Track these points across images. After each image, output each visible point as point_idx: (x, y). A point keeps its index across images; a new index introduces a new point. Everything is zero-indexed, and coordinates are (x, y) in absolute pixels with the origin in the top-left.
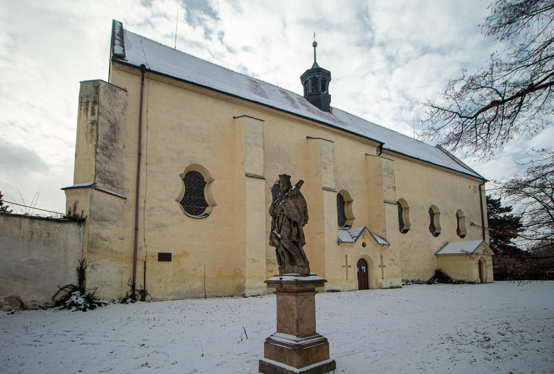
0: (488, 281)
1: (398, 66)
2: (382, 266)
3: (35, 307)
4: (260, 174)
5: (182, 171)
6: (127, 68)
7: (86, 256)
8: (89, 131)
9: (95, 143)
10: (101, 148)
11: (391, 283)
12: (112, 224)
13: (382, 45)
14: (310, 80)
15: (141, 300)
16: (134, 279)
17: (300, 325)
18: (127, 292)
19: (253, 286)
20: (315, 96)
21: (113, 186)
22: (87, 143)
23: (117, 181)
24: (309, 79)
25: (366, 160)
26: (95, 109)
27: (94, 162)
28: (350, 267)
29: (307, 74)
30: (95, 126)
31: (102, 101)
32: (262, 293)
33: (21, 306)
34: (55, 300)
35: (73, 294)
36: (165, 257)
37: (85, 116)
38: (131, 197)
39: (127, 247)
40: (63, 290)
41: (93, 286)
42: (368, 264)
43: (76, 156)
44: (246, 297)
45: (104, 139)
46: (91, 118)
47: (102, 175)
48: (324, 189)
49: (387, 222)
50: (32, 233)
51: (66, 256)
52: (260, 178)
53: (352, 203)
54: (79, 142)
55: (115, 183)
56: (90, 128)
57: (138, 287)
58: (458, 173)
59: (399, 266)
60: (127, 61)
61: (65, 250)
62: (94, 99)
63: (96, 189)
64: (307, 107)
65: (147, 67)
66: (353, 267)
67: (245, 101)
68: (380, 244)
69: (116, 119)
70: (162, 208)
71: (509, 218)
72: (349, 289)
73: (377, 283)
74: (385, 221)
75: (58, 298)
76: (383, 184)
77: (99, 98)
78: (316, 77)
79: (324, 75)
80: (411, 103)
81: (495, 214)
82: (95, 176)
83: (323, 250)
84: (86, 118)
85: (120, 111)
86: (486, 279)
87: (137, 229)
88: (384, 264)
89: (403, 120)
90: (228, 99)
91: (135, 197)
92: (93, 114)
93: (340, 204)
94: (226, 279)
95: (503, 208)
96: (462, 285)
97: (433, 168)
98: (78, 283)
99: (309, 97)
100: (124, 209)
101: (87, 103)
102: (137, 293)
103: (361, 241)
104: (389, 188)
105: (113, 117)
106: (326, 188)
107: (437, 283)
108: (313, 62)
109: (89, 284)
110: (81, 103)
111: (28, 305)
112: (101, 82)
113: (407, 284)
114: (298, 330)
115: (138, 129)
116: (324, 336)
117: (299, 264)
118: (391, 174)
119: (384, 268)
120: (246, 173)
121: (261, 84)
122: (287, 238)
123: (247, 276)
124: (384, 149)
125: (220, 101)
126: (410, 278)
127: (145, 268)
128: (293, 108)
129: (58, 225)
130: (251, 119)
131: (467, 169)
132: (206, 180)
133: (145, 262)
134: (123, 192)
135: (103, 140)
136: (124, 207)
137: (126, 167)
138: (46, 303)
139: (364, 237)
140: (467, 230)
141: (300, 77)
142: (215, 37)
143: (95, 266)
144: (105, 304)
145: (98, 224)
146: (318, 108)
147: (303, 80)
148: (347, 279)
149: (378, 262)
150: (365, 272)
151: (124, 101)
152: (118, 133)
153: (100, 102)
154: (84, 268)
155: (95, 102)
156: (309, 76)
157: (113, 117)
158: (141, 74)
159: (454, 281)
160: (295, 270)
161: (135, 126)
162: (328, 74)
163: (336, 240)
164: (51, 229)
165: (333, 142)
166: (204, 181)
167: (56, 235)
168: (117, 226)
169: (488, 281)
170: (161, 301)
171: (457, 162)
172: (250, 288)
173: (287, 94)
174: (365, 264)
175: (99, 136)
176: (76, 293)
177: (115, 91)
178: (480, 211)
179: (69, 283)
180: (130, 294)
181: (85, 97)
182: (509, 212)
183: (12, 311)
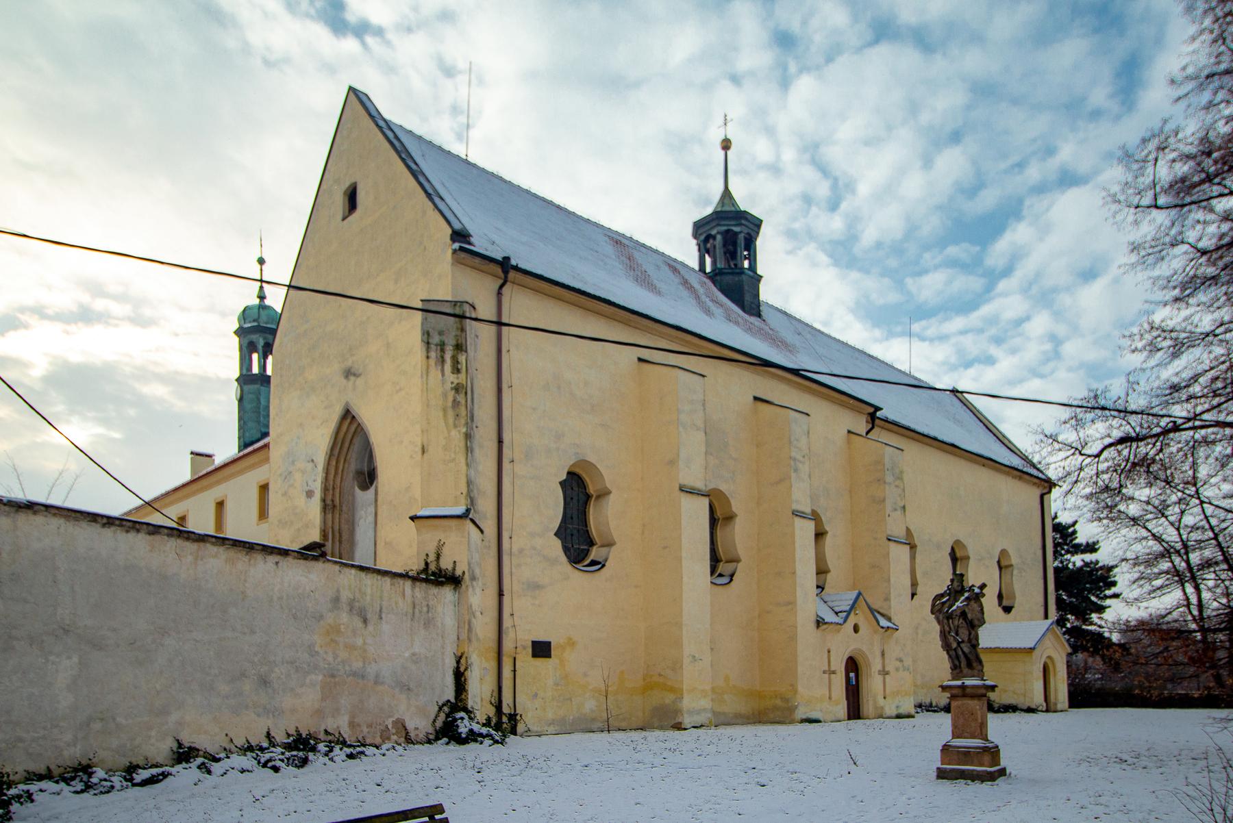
0: (1059, 707)
2: (884, 673)
8: (450, 404)
19: (694, 708)
20: (731, 277)
22: (447, 428)
24: (718, 233)
26: (460, 361)
29: (713, 220)
30: (463, 395)
36: (541, 649)
42: (859, 667)
44: (685, 729)
49: (892, 580)
53: (824, 536)
56: (450, 399)
57: (506, 710)
65: (513, 262)
68: (882, 628)
71: (1089, 567)
72: (834, 719)
73: (876, 708)
74: (889, 581)
78: (732, 230)
79: (750, 228)
80: (835, 186)
81: (1062, 555)
86: (1056, 704)
89: (810, 235)
92: (456, 372)
94: (632, 695)
95: (1080, 545)
101: (442, 346)
104: (895, 510)
106: (798, 511)
119: (887, 676)
120: (680, 485)
130: (686, 373)
140: (1017, 595)
147: (699, 232)
148: (830, 698)
149: (876, 665)
150: (854, 683)
156: (719, 225)
159: (996, 706)
163: (813, 618)
166: (587, 491)
170: (539, 736)
172: (690, 713)
178: (1040, 553)
181: (436, 333)
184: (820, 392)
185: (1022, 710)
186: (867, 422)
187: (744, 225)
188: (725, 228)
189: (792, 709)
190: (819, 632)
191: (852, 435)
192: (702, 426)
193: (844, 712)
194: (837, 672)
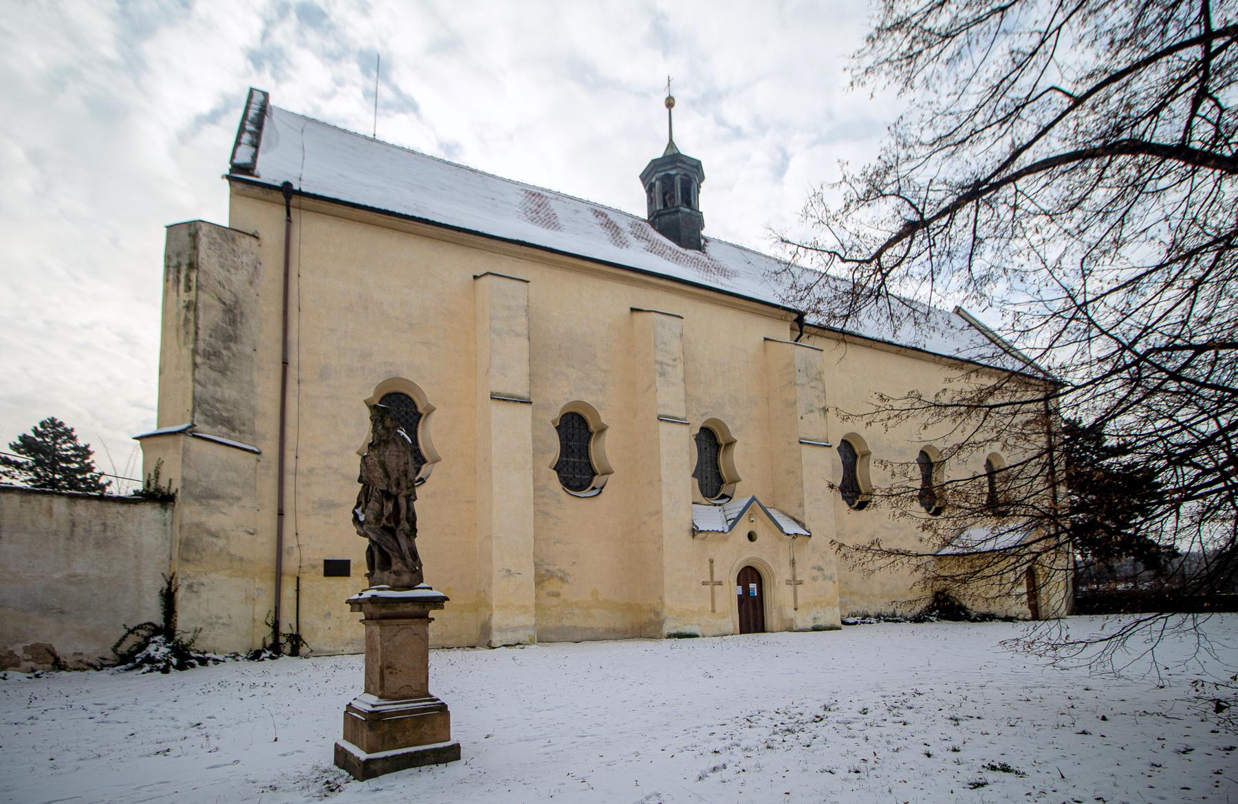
2: (795, 582)
3: (81, 665)
4: (522, 392)
5: (370, 394)
6: (257, 190)
7: (176, 568)
9: (191, 346)
10: (204, 356)
11: (815, 619)
12: (231, 505)
15: (291, 655)
16: (276, 612)
17: (388, 677)
18: (264, 638)
21: (233, 429)
23: (240, 419)
24: (657, 179)
27: (190, 383)
28: (720, 583)
30: (192, 312)
31: (204, 261)
32: (527, 639)
33: (54, 664)
34: (119, 653)
35: (152, 640)
37: (175, 294)
38: (269, 449)
39: (264, 548)
40: (133, 633)
41: (192, 626)
43: (160, 374)
44: (494, 648)
45: (211, 336)
46: (184, 297)
47: (209, 408)
48: (661, 419)
49: (806, 485)
50: (73, 524)
51: (138, 568)
52: (521, 402)
54: (165, 345)
55: (237, 423)
56: (182, 317)
57: (285, 629)
59: (834, 582)
60: (257, 177)
61: (136, 557)
63: (194, 436)
64: (649, 241)
65: (296, 187)
66: (726, 585)
68: (788, 535)
69: (235, 296)
70: (330, 469)
72: (718, 633)
73: (782, 619)
74: (802, 485)
75: (124, 649)
76: (798, 404)
77: (197, 258)
82: (194, 412)
83: (660, 549)
84: (176, 297)
85: (245, 278)
87: (281, 514)
88: (798, 579)
90: (462, 240)
93: (708, 449)
96: (989, 623)
97: (927, 361)
98: (162, 620)
99: (657, 220)
100: (256, 472)
101: (178, 268)
102: (282, 640)
103: (744, 527)
104: (812, 411)
105: (231, 291)
106: (666, 417)
107: (937, 620)
109: (184, 622)
110: (167, 267)
111: (68, 661)
112: (202, 224)
113: (863, 623)
114: (382, 687)
115: (281, 312)
116: (443, 700)
117: (394, 568)
118: (816, 379)
119: (799, 587)
121: (551, 199)
122: (374, 521)
123: (494, 604)
125: (445, 244)
126: (872, 608)
127: (298, 590)
128: (615, 247)
129: (123, 509)
132: (420, 410)
133: (298, 578)
134: (254, 440)
135: (208, 338)
136: (255, 469)
137: (259, 390)
138: (101, 658)
139: (752, 519)
141: (640, 177)
143: (196, 586)
144: (216, 661)
145: (201, 504)
146: (674, 242)
147: (646, 182)
148: (713, 611)
149: (784, 573)
151: (253, 257)
152: (241, 323)
153: (200, 264)
154: (173, 591)
155: (192, 266)
157: (229, 293)
158: (283, 200)
160: (385, 578)
161: (275, 308)
162: (696, 166)
163: (688, 526)
164: (108, 516)
165: (682, 318)
167: (118, 527)
168: (243, 507)
172: (501, 630)
173: (606, 217)
174: (755, 576)
175: (200, 332)
176: (157, 638)
177: (233, 240)
179: (146, 620)
180: (270, 641)
183: (37, 673)
184: (723, 301)
185: (1000, 619)
186: (792, 329)
187: (679, 167)
188: (663, 173)
189: (660, 624)
190: (696, 542)
191: (769, 343)
192: (525, 332)
193: (734, 625)
194: (724, 583)
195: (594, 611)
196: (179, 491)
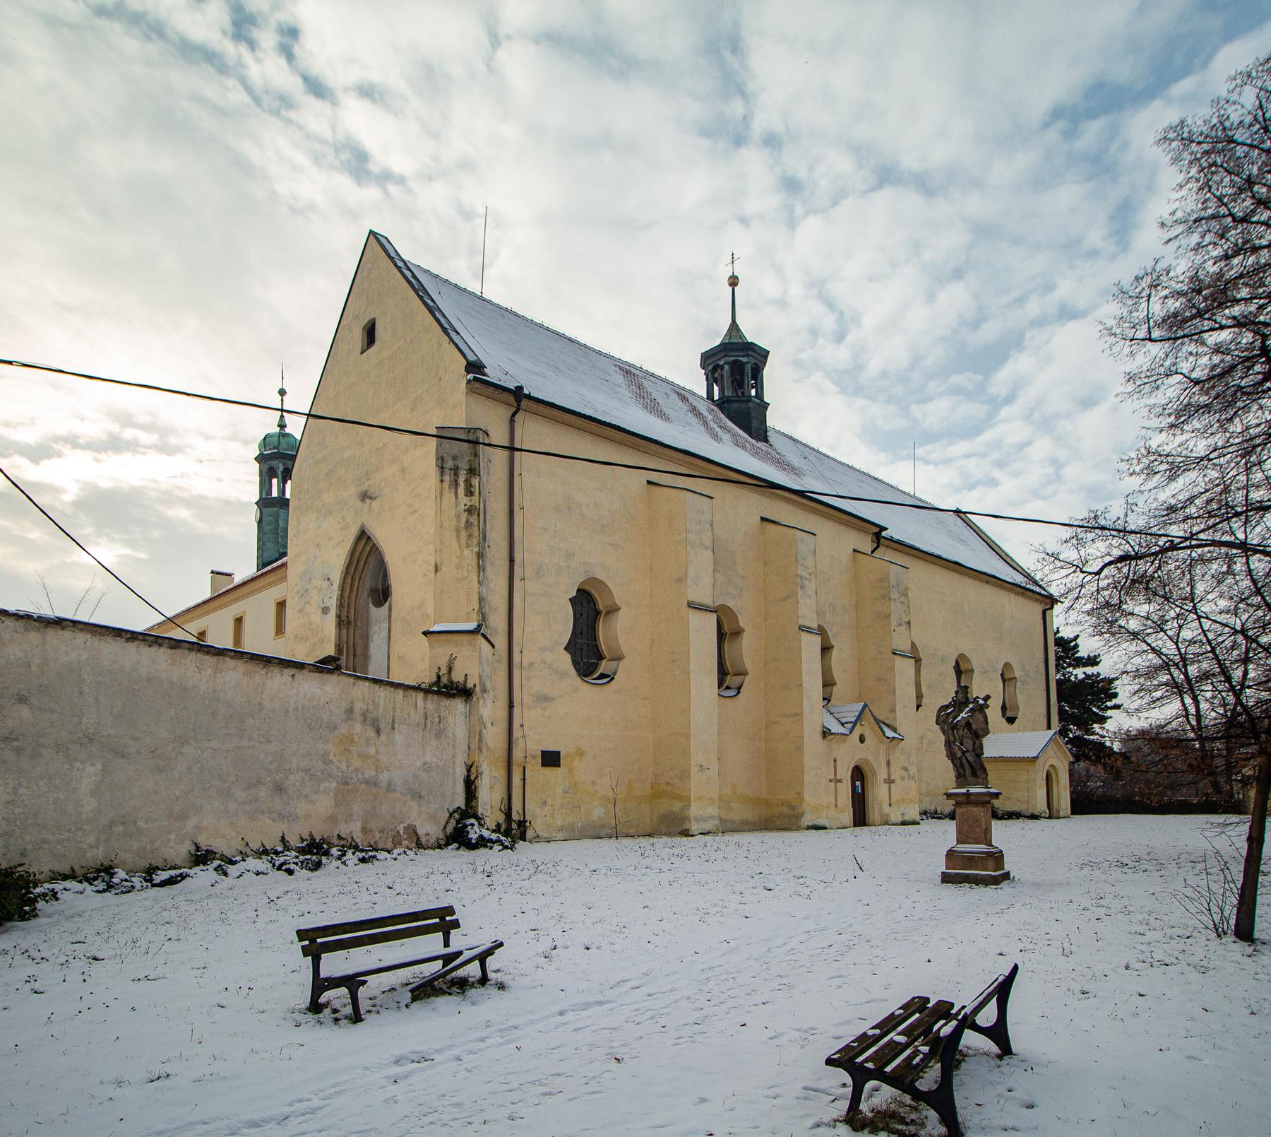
0: (1062, 813)
1: (811, 212)
2: (890, 781)
6: (491, 390)
8: (463, 525)
13: (772, 141)
14: (726, 367)
24: (726, 363)
25: (854, 562)
30: (475, 517)
36: (551, 759)
38: (501, 641)
44: (693, 836)
56: (464, 520)
57: (515, 816)
58: (1006, 585)
62: (471, 465)
67: (670, 450)
68: (888, 738)
73: (882, 815)
81: (1065, 669)
88: (892, 778)
91: (507, 644)
104: (901, 625)
108: (730, 321)
124: (884, 537)
131: (1018, 571)
132: (601, 607)
140: (1020, 707)
142: (268, 39)
148: (836, 806)
149: (882, 774)
156: (725, 356)
159: (1000, 813)
163: (819, 729)
169: (1062, 813)
171: (997, 554)
172: (696, 819)
178: (1042, 666)
182: (1092, 666)
188: (733, 359)
189: (799, 817)
190: (826, 742)
192: (711, 545)
195: (733, 805)
196: (478, 686)
